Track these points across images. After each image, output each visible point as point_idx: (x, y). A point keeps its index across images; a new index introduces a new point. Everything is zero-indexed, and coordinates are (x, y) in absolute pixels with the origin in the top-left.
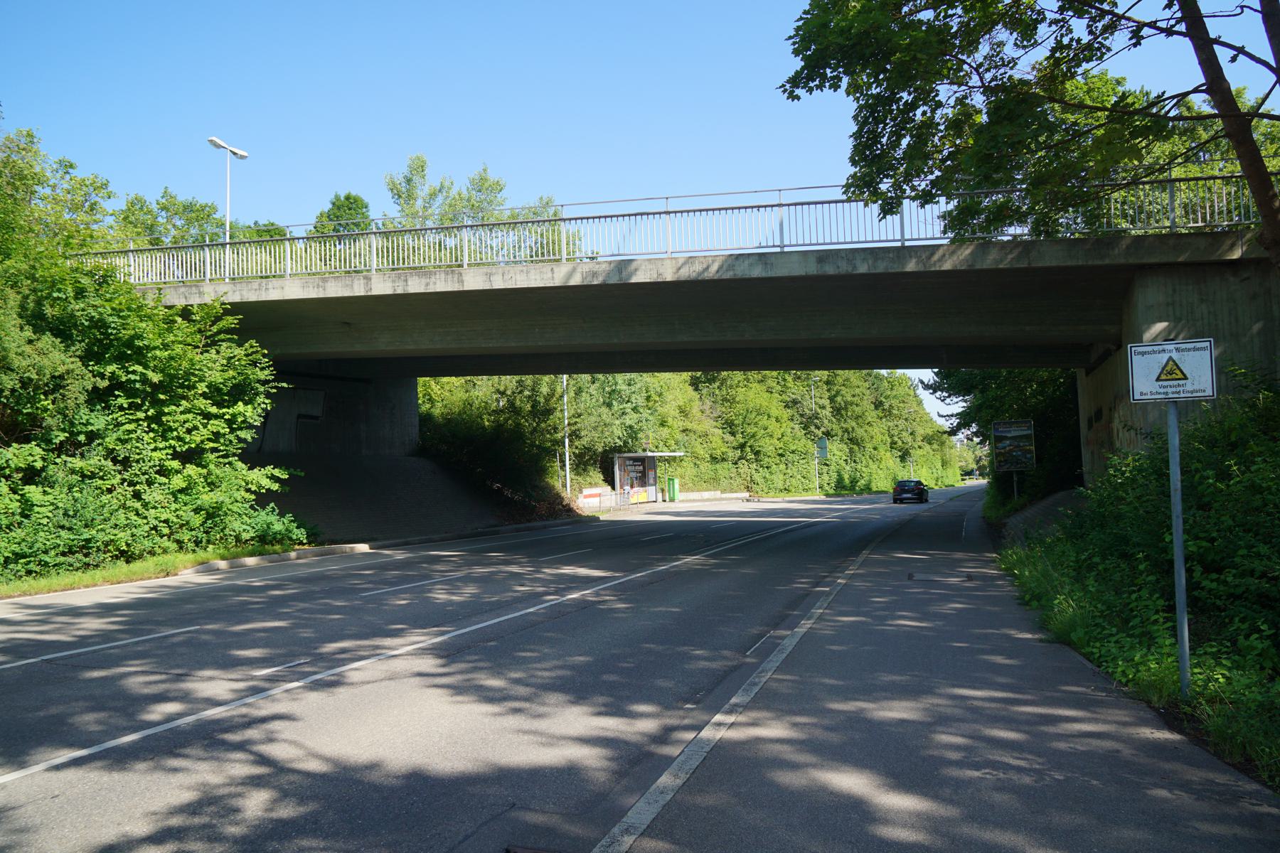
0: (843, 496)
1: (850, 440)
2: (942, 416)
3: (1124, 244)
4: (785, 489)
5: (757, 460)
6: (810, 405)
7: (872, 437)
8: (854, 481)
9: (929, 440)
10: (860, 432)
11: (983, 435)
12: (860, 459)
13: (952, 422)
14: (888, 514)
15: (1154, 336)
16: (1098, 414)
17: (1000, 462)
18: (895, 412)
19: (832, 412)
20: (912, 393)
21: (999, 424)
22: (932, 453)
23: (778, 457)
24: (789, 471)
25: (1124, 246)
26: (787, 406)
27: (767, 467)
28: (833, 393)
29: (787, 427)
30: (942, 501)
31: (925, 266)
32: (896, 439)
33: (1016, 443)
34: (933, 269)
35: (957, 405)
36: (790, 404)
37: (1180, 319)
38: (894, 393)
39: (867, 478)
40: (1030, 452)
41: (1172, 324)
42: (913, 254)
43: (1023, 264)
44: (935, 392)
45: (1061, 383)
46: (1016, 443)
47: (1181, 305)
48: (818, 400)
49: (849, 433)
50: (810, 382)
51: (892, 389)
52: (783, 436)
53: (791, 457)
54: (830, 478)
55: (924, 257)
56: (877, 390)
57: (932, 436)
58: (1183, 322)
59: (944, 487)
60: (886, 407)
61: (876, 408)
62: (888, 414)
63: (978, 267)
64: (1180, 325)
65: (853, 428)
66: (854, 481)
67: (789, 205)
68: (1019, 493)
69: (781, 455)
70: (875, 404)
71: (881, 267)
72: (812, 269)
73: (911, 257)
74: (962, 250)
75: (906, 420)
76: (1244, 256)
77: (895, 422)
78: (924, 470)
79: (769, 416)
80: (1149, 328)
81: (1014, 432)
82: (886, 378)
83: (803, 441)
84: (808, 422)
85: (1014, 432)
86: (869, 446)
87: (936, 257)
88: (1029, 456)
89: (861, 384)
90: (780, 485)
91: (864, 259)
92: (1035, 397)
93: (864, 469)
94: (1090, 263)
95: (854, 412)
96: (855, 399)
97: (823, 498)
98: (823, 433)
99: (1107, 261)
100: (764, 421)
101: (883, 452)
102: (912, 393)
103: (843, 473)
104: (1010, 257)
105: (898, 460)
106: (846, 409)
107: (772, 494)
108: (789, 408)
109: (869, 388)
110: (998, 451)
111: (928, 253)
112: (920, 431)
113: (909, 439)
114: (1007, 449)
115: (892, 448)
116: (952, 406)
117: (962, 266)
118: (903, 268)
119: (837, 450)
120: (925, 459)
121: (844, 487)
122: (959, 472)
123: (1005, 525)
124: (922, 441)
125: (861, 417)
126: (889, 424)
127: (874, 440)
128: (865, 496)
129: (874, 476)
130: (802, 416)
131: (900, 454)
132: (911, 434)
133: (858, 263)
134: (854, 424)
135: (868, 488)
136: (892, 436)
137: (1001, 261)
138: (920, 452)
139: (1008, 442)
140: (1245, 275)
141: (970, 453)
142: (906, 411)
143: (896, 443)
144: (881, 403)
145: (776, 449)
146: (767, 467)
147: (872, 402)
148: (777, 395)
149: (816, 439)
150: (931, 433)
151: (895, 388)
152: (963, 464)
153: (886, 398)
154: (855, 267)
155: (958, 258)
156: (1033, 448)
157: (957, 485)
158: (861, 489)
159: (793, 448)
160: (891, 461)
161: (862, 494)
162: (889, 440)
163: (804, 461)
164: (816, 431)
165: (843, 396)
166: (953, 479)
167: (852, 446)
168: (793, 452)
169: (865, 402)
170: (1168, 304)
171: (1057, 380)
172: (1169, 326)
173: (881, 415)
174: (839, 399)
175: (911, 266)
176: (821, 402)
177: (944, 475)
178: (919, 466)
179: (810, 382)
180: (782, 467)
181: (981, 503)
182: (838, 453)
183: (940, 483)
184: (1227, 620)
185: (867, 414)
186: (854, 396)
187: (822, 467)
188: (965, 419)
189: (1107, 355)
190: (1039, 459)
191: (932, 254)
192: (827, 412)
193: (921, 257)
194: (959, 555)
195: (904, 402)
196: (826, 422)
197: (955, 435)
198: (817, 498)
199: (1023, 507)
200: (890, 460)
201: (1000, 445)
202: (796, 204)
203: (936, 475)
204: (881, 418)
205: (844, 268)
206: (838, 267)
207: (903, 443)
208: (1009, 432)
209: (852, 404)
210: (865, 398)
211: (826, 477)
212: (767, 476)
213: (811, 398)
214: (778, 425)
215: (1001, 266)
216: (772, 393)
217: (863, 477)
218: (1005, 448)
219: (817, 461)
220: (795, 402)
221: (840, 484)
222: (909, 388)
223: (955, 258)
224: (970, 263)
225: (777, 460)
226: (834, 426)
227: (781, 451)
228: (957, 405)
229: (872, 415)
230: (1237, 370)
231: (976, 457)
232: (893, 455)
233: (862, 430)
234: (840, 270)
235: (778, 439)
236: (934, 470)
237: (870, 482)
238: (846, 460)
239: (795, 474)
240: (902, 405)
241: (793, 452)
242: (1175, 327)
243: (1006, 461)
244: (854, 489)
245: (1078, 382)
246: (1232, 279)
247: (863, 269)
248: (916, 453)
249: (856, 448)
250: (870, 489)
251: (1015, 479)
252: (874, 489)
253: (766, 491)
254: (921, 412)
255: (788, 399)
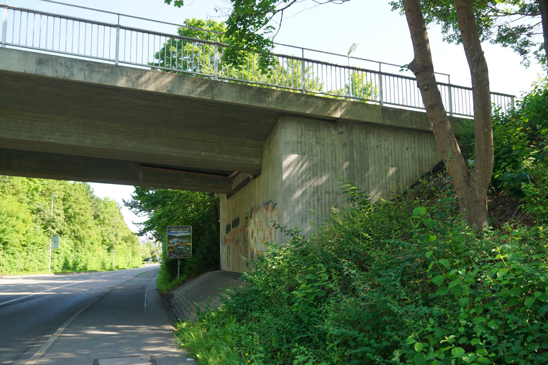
0: (67, 274)
1: (76, 237)
2: (135, 224)
3: (275, 95)
4: (25, 269)
5: (4, 249)
6: (49, 213)
7: (90, 236)
8: (75, 264)
9: (125, 240)
10: (82, 233)
11: (159, 237)
12: (81, 249)
13: (140, 227)
14: (94, 288)
15: (289, 163)
16: (236, 222)
17: (170, 252)
18: (106, 222)
19: (65, 219)
20: (118, 211)
21: (171, 228)
22: (127, 247)
23: (21, 247)
24: (29, 257)
25: (275, 97)
26: (33, 213)
27: (12, 254)
28: (67, 206)
29: (30, 226)
30: (131, 277)
31: (133, 85)
32: (105, 238)
33: (181, 241)
34: (140, 88)
35: (145, 217)
36: (35, 212)
37: (305, 154)
38: (107, 210)
39: (84, 262)
40: (189, 246)
41: (300, 157)
42: (124, 73)
43: (208, 97)
44: (132, 207)
45: (208, 205)
46: (181, 241)
47: (305, 144)
48: (56, 210)
49: (75, 233)
50: (51, 198)
51: (106, 208)
52: (27, 232)
53: (31, 247)
54: (59, 263)
55: (133, 77)
56: (96, 207)
57: (128, 237)
58: (306, 156)
59: (132, 268)
60: (101, 218)
61: (95, 218)
62: (102, 222)
63: (176, 93)
64: (304, 158)
65: (78, 230)
66: (75, 264)
67: (15, 9)
68: (181, 273)
69: (24, 246)
70: (94, 216)
71: (96, 79)
72: (31, 68)
73: (122, 75)
74: (164, 78)
75: (113, 227)
76: (342, 117)
77: (106, 228)
78: (121, 257)
79: (18, 218)
80: (286, 157)
81: (181, 233)
82: (103, 201)
83: (42, 236)
84: (47, 224)
85: (181, 233)
86: (88, 242)
87: (143, 79)
88: (188, 249)
89: (85, 202)
90: (21, 266)
91: (81, 69)
92: (193, 213)
93: (83, 256)
94: (253, 104)
95: (80, 219)
96: (81, 211)
97: (53, 275)
98: (57, 232)
99: (264, 105)
100: (13, 221)
101: (97, 246)
102: (118, 211)
103: (68, 258)
104: (199, 90)
105: (106, 251)
106: (75, 218)
107: (14, 272)
108: (34, 214)
109: (91, 206)
110: (169, 245)
111: (136, 75)
112: (121, 234)
113: (114, 238)
114: (175, 244)
115: (102, 243)
116: (142, 217)
117: (163, 90)
118: (115, 83)
119: (65, 243)
120: (122, 251)
121: (68, 268)
122: (141, 259)
123: (172, 296)
124: (122, 240)
125: (84, 223)
126: (102, 229)
127: (91, 238)
128: (82, 274)
129: (90, 261)
130: (43, 219)
131: (107, 247)
132: (115, 235)
133: (76, 71)
134: (79, 227)
135: (85, 269)
136: (103, 236)
137: (193, 92)
138: (119, 247)
139: (176, 240)
140: (340, 130)
141: (148, 248)
142: (113, 222)
143: (105, 241)
144: (98, 216)
145: (20, 241)
146: (12, 254)
147: (92, 215)
148: (26, 205)
149: (52, 235)
150: (127, 236)
151: (108, 207)
152: (144, 254)
153: (101, 213)
154: (72, 74)
155: (160, 83)
156: (191, 244)
157: (140, 267)
158: (80, 269)
159: (34, 241)
160: (101, 252)
161: (80, 272)
162: (101, 239)
163: (41, 250)
164: (53, 231)
165: (73, 209)
166: (138, 264)
167: (76, 241)
168: (34, 244)
169: (88, 214)
170: (298, 142)
171: (206, 203)
172: (298, 157)
173: (98, 223)
174: (70, 211)
175: (122, 83)
176: (58, 211)
177: (133, 260)
178: (119, 255)
179: (51, 198)
180: (24, 254)
181: (155, 278)
182: (65, 245)
183: (130, 265)
184: (298, 353)
185: (88, 221)
186: (80, 209)
187: (55, 254)
188: (150, 225)
189: (246, 182)
190: (194, 252)
191: (140, 76)
192: (62, 218)
193: (130, 76)
194: (143, 329)
195: (112, 216)
196: (60, 224)
197: (142, 235)
198: (48, 275)
199: (184, 282)
200: (101, 251)
201: (171, 242)
202: (22, 10)
203: (128, 261)
204: (97, 225)
205: (62, 73)
206: (57, 71)
207: (110, 241)
208: (178, 233)
209: (78, 214)
210: (88, 211)
211: (56, 261)
212: (11, 260)
213: (51, 208)
214: (24, 224)
215: (192, 96)
216: (21, 202)
217: (82, 262)
218: (174, 243)
219: (51, 250)
220: (39, 210)
221: (66, 266)
222: (116, 209)
223: (158, 83)
224: (169, 89)
225: (21, 249)
226: (66, 228)
227: (24, 243)
228: (145, 217)
229: (91, 222)
230: (187, 242)
231: (151, 251)
232: (103, 248)
233: (84, 231)
234: (59, 74)
235: (23, 235)
236: (127, 258)
237: (86, 264)
238: (72, 250)
239: (34, 259)
240: (111, 218)
241: (34, 244)
242: (302, 159)
243: (174, 252)
244: (75, 269)
245: (221, 203)
246: (333, 131)
247: (79, 76)
248: (117, 247)
249: (79, 242)
250: (86, 269)
251: (179, 264)
252: (89, 269)
253: (9, 270)
254: (122, 223)
255: (34, 208)
